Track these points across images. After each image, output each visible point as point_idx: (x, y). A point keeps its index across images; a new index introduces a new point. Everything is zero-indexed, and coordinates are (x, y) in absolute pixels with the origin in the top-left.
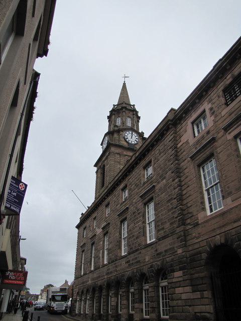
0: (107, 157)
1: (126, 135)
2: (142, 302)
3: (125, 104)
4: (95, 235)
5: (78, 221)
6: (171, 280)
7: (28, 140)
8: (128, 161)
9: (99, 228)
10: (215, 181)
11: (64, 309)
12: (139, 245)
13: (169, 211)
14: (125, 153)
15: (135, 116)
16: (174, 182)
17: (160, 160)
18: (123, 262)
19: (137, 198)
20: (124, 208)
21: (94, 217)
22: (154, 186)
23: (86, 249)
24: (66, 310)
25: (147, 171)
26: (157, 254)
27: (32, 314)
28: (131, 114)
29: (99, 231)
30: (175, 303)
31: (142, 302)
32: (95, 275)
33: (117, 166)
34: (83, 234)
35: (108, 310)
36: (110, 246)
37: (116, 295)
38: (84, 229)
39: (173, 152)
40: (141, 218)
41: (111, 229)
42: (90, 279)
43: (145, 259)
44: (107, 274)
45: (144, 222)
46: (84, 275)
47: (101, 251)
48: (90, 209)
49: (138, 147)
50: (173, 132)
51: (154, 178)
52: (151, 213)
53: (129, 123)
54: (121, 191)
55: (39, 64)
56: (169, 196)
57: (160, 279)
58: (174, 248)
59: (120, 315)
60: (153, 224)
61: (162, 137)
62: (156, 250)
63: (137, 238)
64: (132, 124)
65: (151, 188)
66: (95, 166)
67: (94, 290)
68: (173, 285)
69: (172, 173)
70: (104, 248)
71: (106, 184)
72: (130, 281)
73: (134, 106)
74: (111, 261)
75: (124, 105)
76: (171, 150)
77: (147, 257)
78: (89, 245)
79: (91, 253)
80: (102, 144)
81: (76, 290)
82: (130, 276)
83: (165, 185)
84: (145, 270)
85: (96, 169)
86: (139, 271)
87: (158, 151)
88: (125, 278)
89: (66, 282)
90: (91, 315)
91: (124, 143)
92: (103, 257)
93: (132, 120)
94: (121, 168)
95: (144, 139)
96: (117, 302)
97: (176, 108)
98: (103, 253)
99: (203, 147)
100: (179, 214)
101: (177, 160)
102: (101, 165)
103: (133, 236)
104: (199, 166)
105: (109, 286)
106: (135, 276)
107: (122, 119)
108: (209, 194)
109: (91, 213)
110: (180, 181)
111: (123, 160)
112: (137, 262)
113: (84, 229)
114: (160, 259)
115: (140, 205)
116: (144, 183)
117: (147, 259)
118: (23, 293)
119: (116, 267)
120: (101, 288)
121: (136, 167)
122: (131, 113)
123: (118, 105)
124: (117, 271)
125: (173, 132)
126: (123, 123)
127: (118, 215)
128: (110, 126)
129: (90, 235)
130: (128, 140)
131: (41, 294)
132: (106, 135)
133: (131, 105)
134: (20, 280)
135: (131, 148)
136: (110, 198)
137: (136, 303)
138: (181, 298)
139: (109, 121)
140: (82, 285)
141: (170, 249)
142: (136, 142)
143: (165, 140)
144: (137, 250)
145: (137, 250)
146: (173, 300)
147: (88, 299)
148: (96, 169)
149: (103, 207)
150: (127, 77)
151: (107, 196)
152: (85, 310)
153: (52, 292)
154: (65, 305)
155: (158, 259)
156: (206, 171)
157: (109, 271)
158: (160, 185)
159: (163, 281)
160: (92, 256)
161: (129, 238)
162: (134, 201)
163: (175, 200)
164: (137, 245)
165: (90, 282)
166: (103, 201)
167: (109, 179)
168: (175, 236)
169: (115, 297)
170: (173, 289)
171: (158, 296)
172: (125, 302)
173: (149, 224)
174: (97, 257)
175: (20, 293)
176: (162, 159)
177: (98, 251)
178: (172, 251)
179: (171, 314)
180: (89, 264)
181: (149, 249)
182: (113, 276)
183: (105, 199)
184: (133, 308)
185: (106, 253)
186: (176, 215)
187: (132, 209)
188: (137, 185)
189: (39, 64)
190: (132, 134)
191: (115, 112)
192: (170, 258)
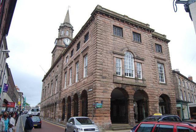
55: (8, 61)
64: (69, 35)
66: (52, 53)
78: (54, 80)
80: (55, 43)
110: (62, 76)
122: (69, 29)
139: (59, 31)
140: (82, 86)
173: (85, 67)
185: (77, 75)
189: (8, 61)
191: (61, 28)
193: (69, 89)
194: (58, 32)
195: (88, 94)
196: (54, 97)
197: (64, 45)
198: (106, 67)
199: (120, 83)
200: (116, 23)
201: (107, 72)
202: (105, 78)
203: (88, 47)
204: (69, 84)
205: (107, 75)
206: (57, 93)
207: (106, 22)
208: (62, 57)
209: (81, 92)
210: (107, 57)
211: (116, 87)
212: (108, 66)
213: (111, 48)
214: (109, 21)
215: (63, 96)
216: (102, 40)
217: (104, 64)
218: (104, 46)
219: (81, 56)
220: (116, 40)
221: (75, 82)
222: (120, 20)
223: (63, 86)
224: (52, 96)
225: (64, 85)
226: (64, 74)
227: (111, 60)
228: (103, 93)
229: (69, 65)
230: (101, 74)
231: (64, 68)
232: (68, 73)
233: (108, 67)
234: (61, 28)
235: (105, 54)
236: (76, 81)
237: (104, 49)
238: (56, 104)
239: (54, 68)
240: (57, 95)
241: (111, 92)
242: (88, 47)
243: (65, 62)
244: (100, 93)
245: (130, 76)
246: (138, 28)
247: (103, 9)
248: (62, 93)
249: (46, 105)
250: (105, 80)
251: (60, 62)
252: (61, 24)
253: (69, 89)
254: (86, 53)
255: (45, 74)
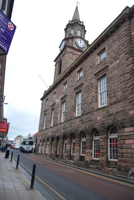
0: (64, 55)
1: (77, 41)
2: (92, 149)
3: (77, 20)
4: (55, 103)
5: (42, 96)
6: (122, 133)
7: (13, 7)
8: (77, 59)
9: (58, 99)
10: (105, 89)
11: (31, 149)
12: (92, 109)
13: (121, 83)
14: (76, 53)
15: (83, 29)
16: (128, 61)
17: (114, 47)
18: (77, 121)
19: (91, 76)
20: (79, 84)
21: (54, 92)
22: (107, 66)
23: (47, 113)
24: (32, 151)
25: (79, 74)
26: (108, 115)
27: (12, 152)
28: (80, 28)
29: (58, 101)
30: (124, 151)
31: (92, 149)
32: (54, 130)
33: (70, 60)
34: (46, 104)
35: (57, 151)
36: (67, 111)
37: (70, 142)
38: (46, 100)
39: (128, 38)
40: (94, 90)
41: (67, 99)
42: (50, 132)
43: (97, 119)
44: (64, 129)
45: (97, 92)
46: (45, 129)
47: (59, 114)
48: (51, 88)
49: (84, 50)
50: (128, 23)
51: (108, 60)
52: (103, 86)
53: (79, 34)
54: (77, 73)
56: (122, 72)
57: (94, 135)
58: (126, 110)
59: (73, 156)
60: (80, 106)
61: (117, 29)
62: (108, 112)
63: (90, 104)
64: (82, 34)
65: (105, 67)
66: (55, 61)
67: (53, 139)
68: (123, 138)
69: (126, 54)
70: (61, 112)
71: (63, 69)
72: (83, 134)
73: (83, 22)
74: (67, 121)
75: (76, 21)
76: (125, 37)
77: (99, 117)
79: (51, 115)
80: (60, 47)
81: (39, 139)
82: (83, 130)
83: (119, 64)
84: (97, 126)
85: (55, 63)
86: (91, 127)
87: (112, 40)
88: (79, 131)
89: (30, 134)
90: (50, 154)
91: (76, 47)
92: (61, 118)
93: (81, 32)
94: (73, 62)
95: (88, 45)
96: (71, 148)
97: (130, 7)
98: (61, 115)
99: (77, 87)
100: (132, 84)
101: (131, 44)
102: (59, 61)
103: (87, 103)
104: (98, 80)
105: (65, 137)
106: (88, 130)
107: (75, 31)
108: (101, 96)
109: (52, 90)
111: (75, 57)
112: (90, 121)
113: (46, 100)
114: (111, 118)
115: (94, 81)
116: (98, 65)
117: (99, 118)
118: (5, 139)
119: (71, 124)
120: (58, 138)
121: (91, 54)
122: (81, 27)
123: (72, 21)
124: (71, 127)
125: (128, 23)
126: (75, 33)
127: (74, 89)
128: (66, 35)
129: (51, 104)
130: (78, 44)
131: (15, 141)
132: (63, 40)
133: (80, 22)
134: (4, 129)
135: (79, 50)
136: (67, 78)
137: (88, 149)
138: (131, 147)
140: (43, 136)
141: (121, 111)
142: (83, 46)
143: (120, 31)
144: (90, 112)
145: (90, 112)
146: (122, 148)
147: (48, 145)
148: (55, 63)
149: (61, 85)
150: (78, 3)
151: (65, 77)
152: (46, 151)
153: (24, 139)
154: (32, 147)
155: (109, 119)
156: (101, 83)
157: (65, 127)
158: (113, 64)
159: (95, 137)
160: (44, 121)
161: (82, 104)
162: (88, 78)
163: (129, 74)
164: (90, 109)
165: (50, 134)
166: (62, 81)
167: (65, 69)
168: (127, 101)
169: (69, 144)
170: (123, 141)
171: (107, 145)
172: (78, 148)
173: (63, 113)
174: (56, 118)
175: (3, 139)
176: (115, 46)
177: (57, 114)
178: (124, 112)
179: (119, 158)
180: (49, 122)
181: (100, 111)
182: (68, 130)
183: (63, 79)
184: (83, 152)
186: (129, 85)
187: (86, 84)
188: (91, 67)
190: (81, 40)
192: (122, 118)
194: (64, 34)
234: (69, 26)
239: (84, 63)
247: (106, 30)
254: (80, 90)
255: (47, 89)
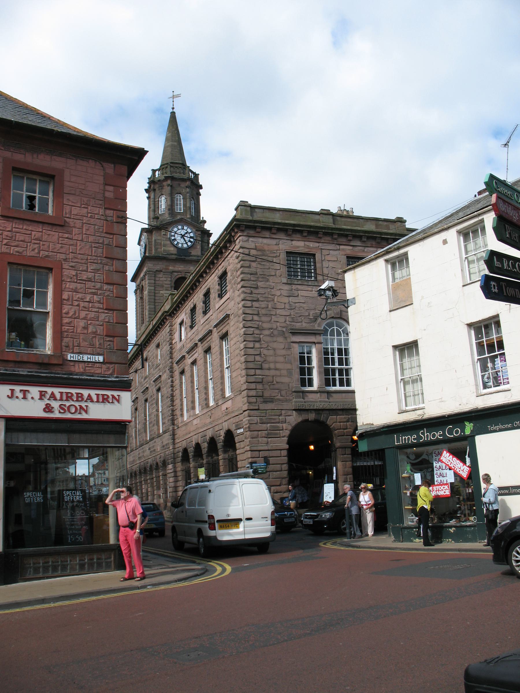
78: (153, 390)
80: (139, 244)
139: (149, 198)
189: (216, 519)
193: (195, 422)
195: (237, 439)
196: (158, 445)
197: (172, 249)
198: (272, 372)
199: (312, 408)
200: (295, 243)
201: (277, 386)
202: (271, 400)
203: (227, 316)
204: (193, 408)
205: (275, 393)
206: (164, 432)
207: (266, 248)
208: (167, 320)
209: (222, 433)
210: (275, 345)
211: (300, 419)
212: (276, 369)
213: (282, 319)
214: (274, 242)
215: (181, 444)
216: (255, 304)
217: (265, 366)
218: (264, 319)
219: (216, 336)
220: (296, 293)
221: (207, 405)
222: (305, 234)
223: (178, 412)
224: (151, 440)
225: (182, 410)
226: (177, 374)
227: (284, 352)
228: (266, 438)
229: (188, 352)
230: (261, 394)
231: (177, 356)
232: (188, 373)
233: (278, 373)
235: (268, 339)
236: (212, 403)
237: (265, 325)
238: (165, 464)
240: (167, 439)
241: (287, 433)
242: (227, 316)
243: (176, 336)
244: (260, 439)
245: (341, 384)
246: (364, 242)
248: (180, 433)
249: (136, 468)
250: (269, 406)
251: (163, 335)
252: (154, 171)
253: (195, 422)
